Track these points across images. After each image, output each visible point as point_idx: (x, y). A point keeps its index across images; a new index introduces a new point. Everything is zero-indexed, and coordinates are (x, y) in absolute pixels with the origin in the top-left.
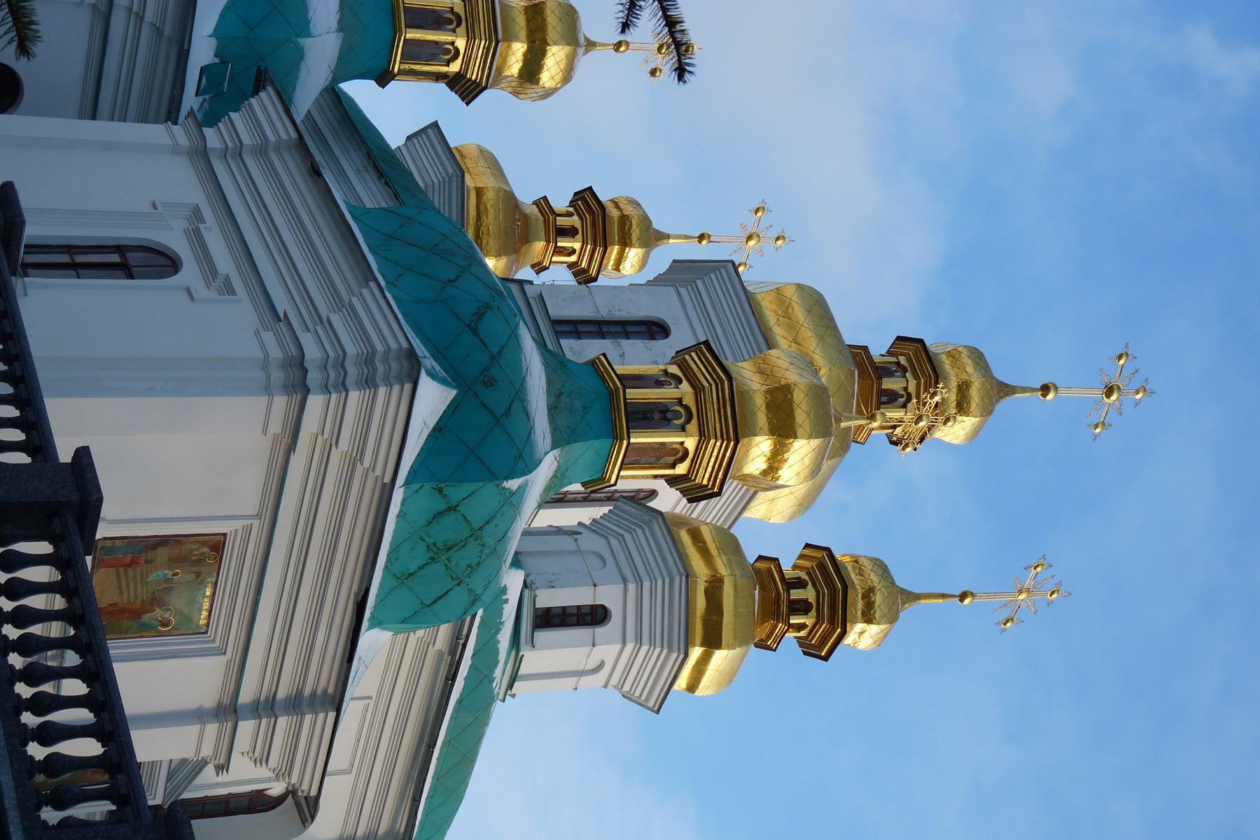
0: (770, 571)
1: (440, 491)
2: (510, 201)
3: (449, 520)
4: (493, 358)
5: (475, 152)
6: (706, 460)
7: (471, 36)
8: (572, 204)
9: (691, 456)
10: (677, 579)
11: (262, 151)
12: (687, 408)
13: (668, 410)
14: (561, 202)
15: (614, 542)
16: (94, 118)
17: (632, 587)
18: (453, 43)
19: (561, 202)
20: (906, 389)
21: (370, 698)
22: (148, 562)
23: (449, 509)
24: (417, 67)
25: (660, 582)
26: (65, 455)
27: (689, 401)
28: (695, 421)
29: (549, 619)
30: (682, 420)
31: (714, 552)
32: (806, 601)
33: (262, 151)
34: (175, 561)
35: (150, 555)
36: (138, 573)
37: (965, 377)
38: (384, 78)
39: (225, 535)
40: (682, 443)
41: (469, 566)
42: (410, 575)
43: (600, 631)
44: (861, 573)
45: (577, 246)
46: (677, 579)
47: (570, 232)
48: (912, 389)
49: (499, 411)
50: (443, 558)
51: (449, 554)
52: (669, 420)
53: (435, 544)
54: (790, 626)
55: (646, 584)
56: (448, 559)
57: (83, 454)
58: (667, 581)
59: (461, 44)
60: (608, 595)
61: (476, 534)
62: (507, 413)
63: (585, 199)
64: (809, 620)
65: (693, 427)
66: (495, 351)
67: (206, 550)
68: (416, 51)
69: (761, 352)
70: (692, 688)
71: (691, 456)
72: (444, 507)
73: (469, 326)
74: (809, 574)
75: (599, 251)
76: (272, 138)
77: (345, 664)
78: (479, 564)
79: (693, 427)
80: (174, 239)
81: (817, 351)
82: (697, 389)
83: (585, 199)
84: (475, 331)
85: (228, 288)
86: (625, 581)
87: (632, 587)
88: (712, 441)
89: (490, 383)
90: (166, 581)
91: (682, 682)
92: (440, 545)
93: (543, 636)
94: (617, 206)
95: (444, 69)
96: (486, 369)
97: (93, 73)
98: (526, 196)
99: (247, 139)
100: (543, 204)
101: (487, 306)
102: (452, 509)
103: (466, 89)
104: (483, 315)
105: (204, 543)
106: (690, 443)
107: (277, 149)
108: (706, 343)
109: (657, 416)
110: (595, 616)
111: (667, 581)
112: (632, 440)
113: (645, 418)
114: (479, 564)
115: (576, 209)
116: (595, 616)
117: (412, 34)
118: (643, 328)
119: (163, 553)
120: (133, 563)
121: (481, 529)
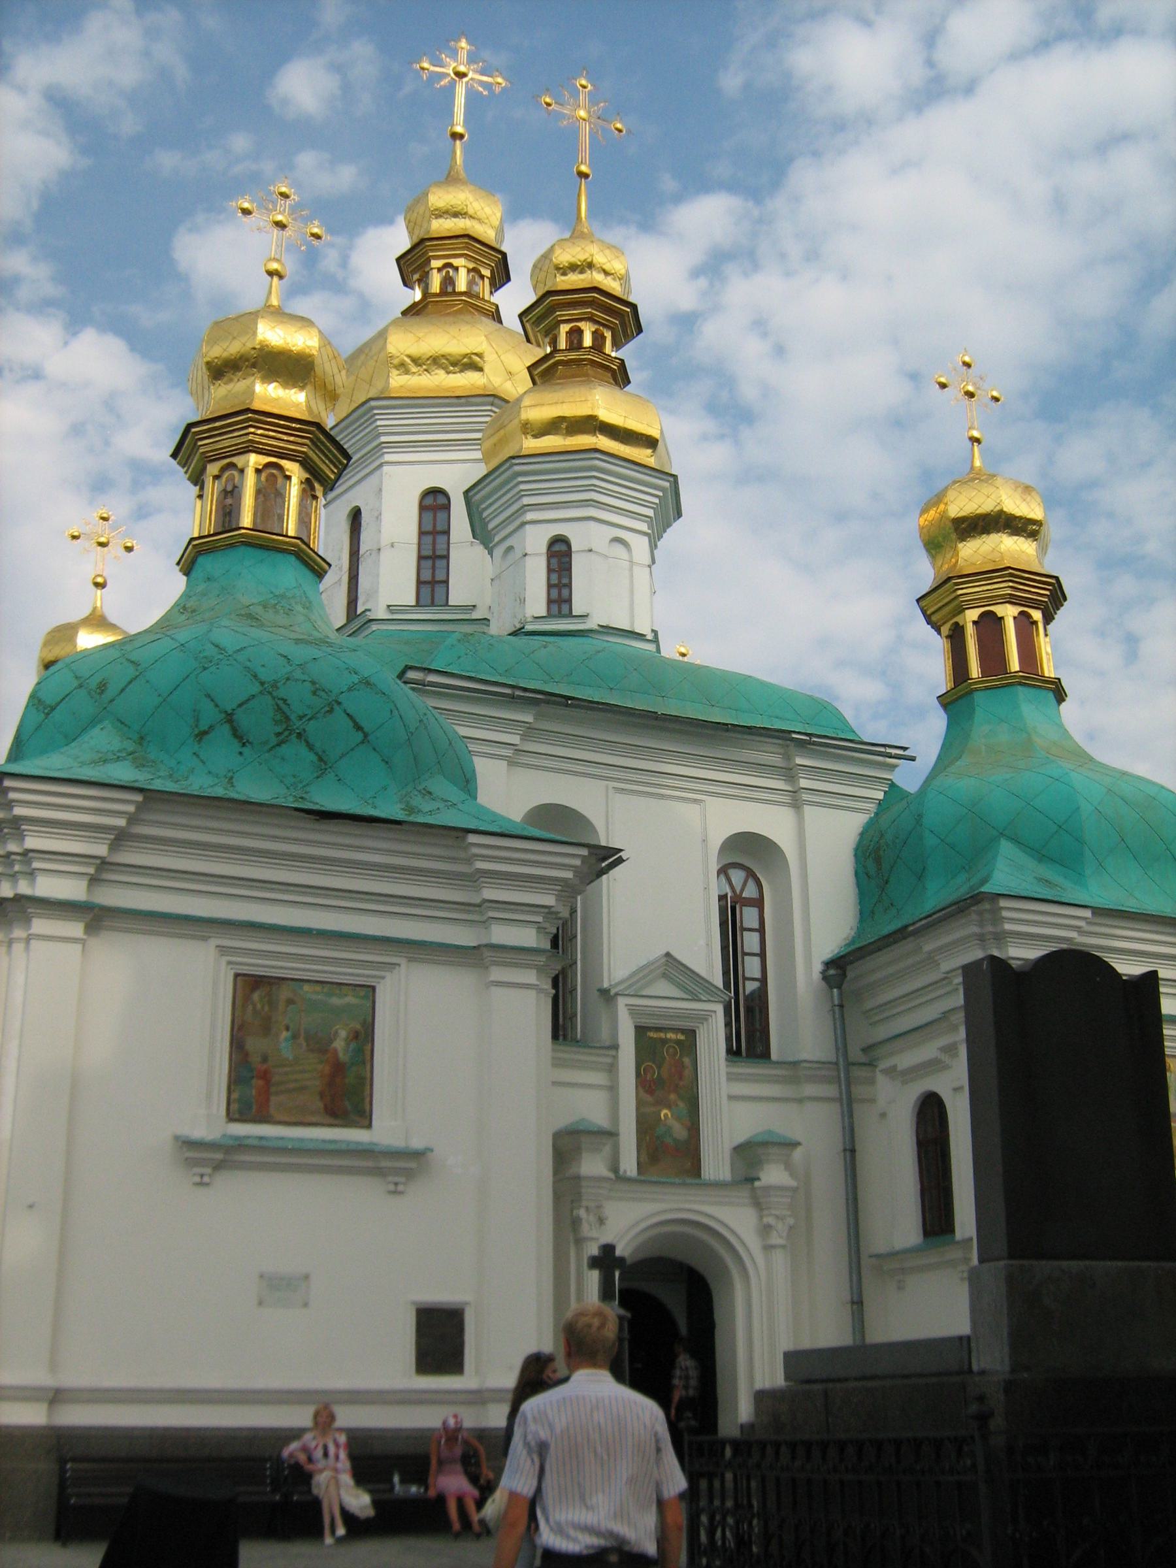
3: (244, 720)
10: (517, 468)
20: (439, 270)
21: (607, 787)
22: (265, 1059)
25: (522, 487)
28: (234, 460)
29: (560, 594)
30: (235, 473)
32: (570, 333)
34: (267, 1028)
35: (255, 1059)
41: (314, 693)
42: (321, 759)
49: (131, 672)
50: (298, 723)
51: (293, 717)
52: (235, 487)
53: (278, 734)
55: (526, 501)
56: (301, 718)
58: (520, 479)
60: (536, 540)
61: (269, 688)
62: (136, 664)
64: (588, 330)
65: (239, 461)
66: (76, 683)
67: (256, 996)
72: (227, 727)
73: (48, 714)
76: (569, 875)
77: (404, 827)
78: (313, 683)
79: (239, 461)
84: (53, 709)
86: (523, 524)
87: (530, 516)
89: (102, 687)
90: (295, 1037)
91: (641, 454)
92: (279, 729)
102: (229, 718)
104: (40, 701)
105: (247, 999)
109: (229, 501)
110: (560, 554)
111: (520, 479)
112: (291, 533)
113: (230, 513)
114: (313, 683)
116: (560, 554)
119: (255, 1044)
120: (265, 1076)
121: (262, 684)
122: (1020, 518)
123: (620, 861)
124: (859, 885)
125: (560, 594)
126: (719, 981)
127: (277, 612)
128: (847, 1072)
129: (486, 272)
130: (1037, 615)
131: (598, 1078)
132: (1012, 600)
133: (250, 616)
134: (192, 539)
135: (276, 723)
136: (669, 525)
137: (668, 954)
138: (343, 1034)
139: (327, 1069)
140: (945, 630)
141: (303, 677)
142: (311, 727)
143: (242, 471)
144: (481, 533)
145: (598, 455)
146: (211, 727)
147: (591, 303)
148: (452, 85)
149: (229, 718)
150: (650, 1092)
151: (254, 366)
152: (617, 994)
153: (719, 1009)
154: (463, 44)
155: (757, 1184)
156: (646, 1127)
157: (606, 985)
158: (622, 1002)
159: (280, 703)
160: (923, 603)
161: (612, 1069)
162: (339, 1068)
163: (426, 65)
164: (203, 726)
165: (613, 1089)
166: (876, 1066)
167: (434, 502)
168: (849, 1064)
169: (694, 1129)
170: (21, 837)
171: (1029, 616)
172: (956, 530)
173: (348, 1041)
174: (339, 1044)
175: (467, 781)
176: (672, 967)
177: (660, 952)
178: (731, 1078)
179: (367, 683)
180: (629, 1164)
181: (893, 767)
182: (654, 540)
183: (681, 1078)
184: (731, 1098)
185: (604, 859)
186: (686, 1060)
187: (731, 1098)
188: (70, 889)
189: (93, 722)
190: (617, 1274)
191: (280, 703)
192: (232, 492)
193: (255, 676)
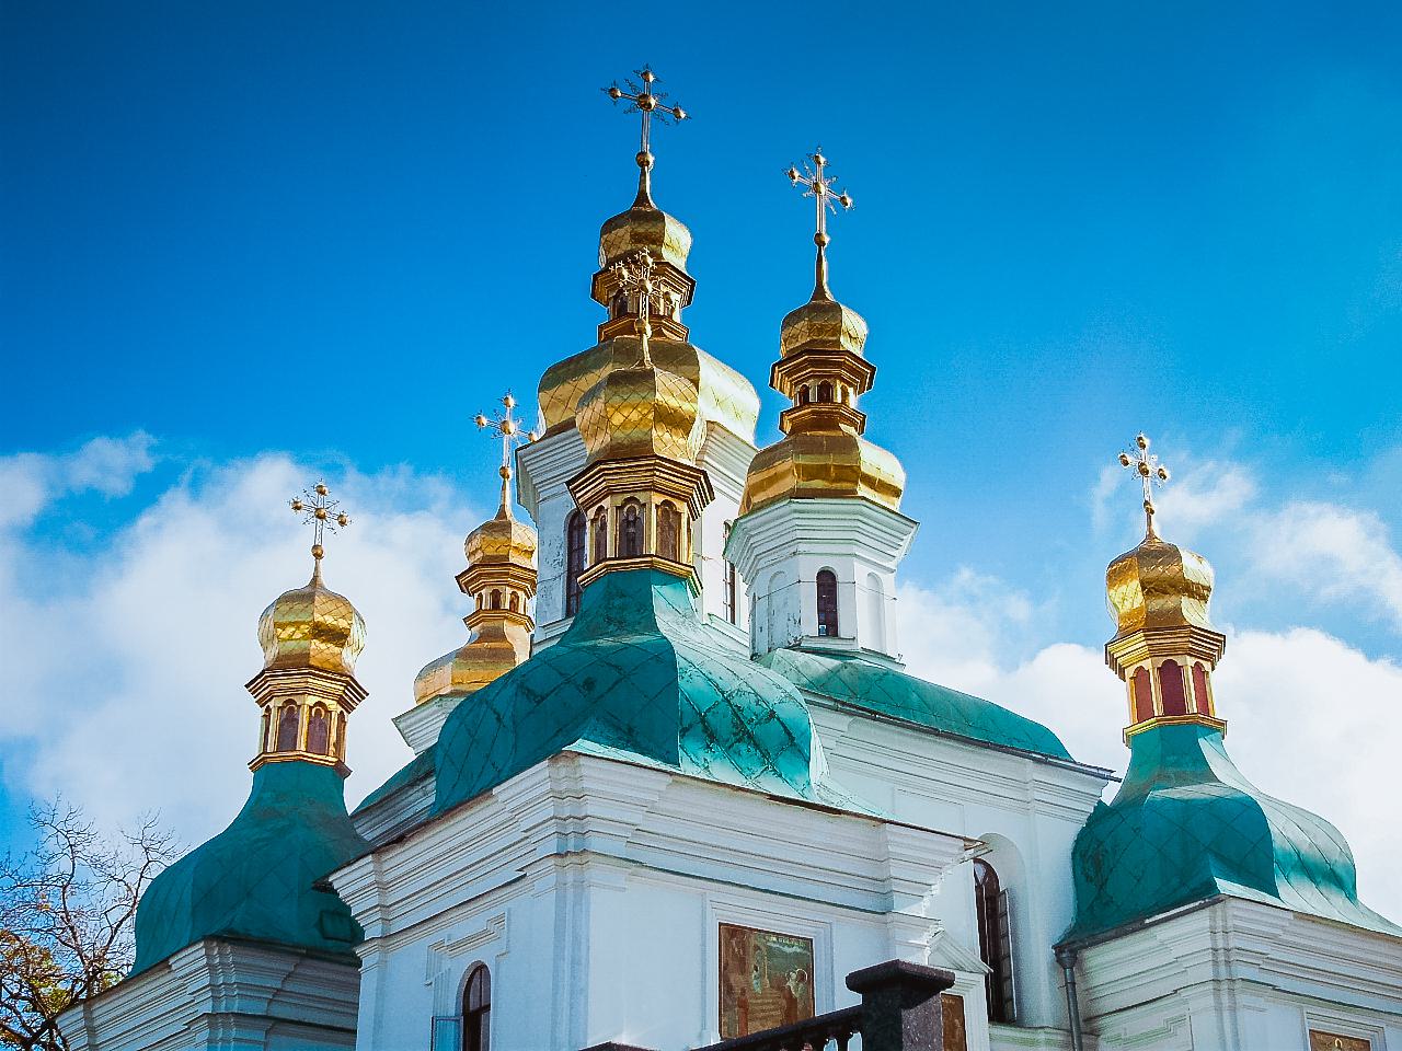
0: (791, 420)
2: (464, 655)
4: (568, 681)
5: (421, 684)
6: (669, 484)
7: (306, 692)
8: (471, 594)
9: (669, 498)
11: (383, 887)
12: (628, 501)
13: (627, 519)
14: (469, 604)
15: (762, 564)
16: (354, 1032)
18: (311, 708)
19: (469, 604)
21: (893, 789)
22: (743, 991)
24: (333, 738)
26: (855, 999)
27: (619, 500)
31: (772, 472)
33: (383, 887)
34: (743, 970)
37: (628, 237)
38: (341, 771)
39: (720, 924)
40: (657, 506)
43: (840, 578)
44: (795, 337)
45: (509, 590)
46: (794, 506)
47: (496, 596)
49: (615, 675)
52: (636, 518)
53: (735, 734)
54: (843, 402)
57: (854, 982)
59: (311, 700)
60: (808, 571)
63: (466, 582)
65: (642, 497)
68: (318, 741)
69: (789, 374)
71: (669, 498)
72: (700, 725)
73: (539, 702)
74: (796, 384)
75: (514, 571)
78: (756, 694)
80: (457, 969)
81: (597, 372)
82: (610, 492)
83: (466, 582)
84: (543, 699)
85: (499, 920)
87: (802, 547)
88: (655, 478)
89: (589, 684)
94: (473, 553)
95: (335, 716)
96: (577, 687)
97: (326, 1034)
98: (462, 637)
99: (375, 901)
100: (470, 621)
101: (521, 686)
103: (352, 694)
104: (529, 690)
105: (728, 944)
106: (658, 499)
107: (382, 873)
108: (568, 483)
109: (632, 530)
110: (827, 583)
112: (653, 552)
113: (633, 540)
115: (475, 592)
116: (827, 583)
117: (302, 746)
118: (575, 533)
119: (736, 979)
120: (743, 1005)
124: (1076, 884)
128: (1080, 1039)
135: (735, 725)
138: (794, 976)
140: (1130, 672)
145: (864, 502)
146: (691, 726)
162: (792, 1001)
164: (686, 724)
166: (1099, 1036)
172: (1143, 588)
174: (791, 984)
183: (953, 1037)
192: (634, 522)
193: (717, 686)
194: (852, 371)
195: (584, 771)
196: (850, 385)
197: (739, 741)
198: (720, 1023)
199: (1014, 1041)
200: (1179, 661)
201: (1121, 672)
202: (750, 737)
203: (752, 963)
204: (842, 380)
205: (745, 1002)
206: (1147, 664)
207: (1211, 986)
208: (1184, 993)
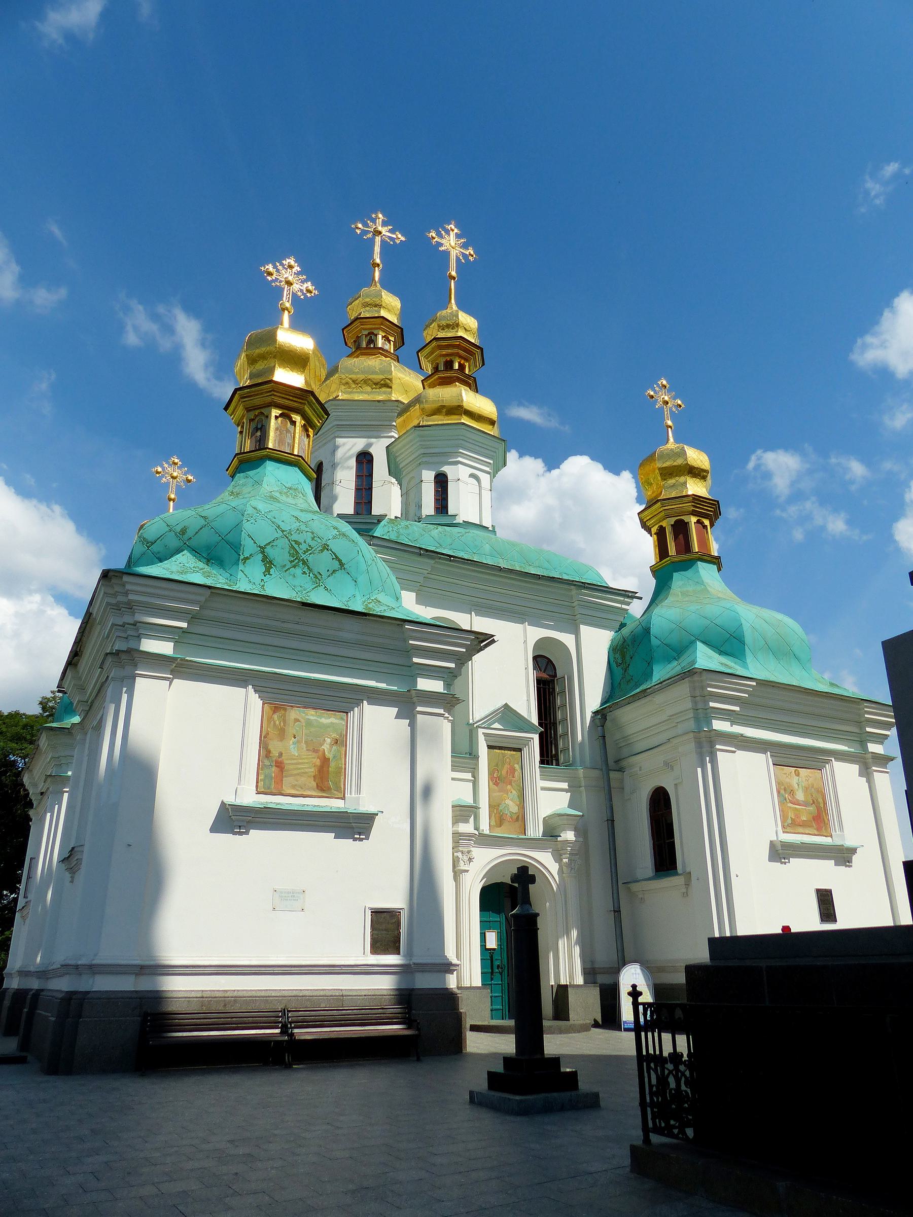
1: (246, 559)
17: (460, 459)
20: (366, 336)
22: (281, 754)
23: (263, 552)
28: (263, 410)
29: (442, 504)
34: (282, 734)
35: (275, 753)
36: (290, 762)
40: (276, 417)
42: (316, 577)
48: (366, 332)
49: (203, 522)
51: (300, 552)
53: (291, 562)
61: (286, 534)
62: (205, 518)
66: (167, 529)
67: (275, 716)
70: (492, 423)
78: (313, 533)
84: (152, 543)
89: (183, 531)
93: (451, 511)
105: (270, 719)
110: (441, 482)
112: (296, 453)
114: (313, 533)
119: (275, 747)
120: (280, 765)
121: (283, 531)
122: (697, 468)
123: (493, 641)
125: (442, 504)
126: (535, 720)
127: (288, 496)
129: (392, 339)
130: (707, 522)
131: (469, 776)
132: (694, 513)
133: (272, 497)
134: (237, 454)
135: (291, 555)
136: (499, 470)
137: (506, 706)
138: (328, 740)
139: (318, 762)
140: (654, 530)
141: (307, 529)
142: (310, 559)
143: (267, 417)
144: (394, 470)
147: (458, 347)
148: (372, 241)
149: (262, 549)
150: (496, 784)
151: (275, 357)
152: (478, 727)
153: (536, 738)
154: (380, 216)
155: (559, 839)
156: (493, 807)
157: (471, 721)
158: (481, 731)
159: (293, 543)
160: (642, 515)
161: (474, 771)
162: (325, 761)
163: (360, 226)
165: (475, 783)
167: (365, 459)
168: (609, 770)
169: (522, 807)
170: (133, 614)
171: (702, 523)
173: (331, 745)
174: (326, 747)
175: (397, 599)
176: (507, 715)
177: (500, 704)
178: (544, 777)
179: (344, 535)
180: (485, 827)
181: (628, 604)
182: (493, 474)
184: (543, 789)
185: (483, 641)
186: (517, 767)
187: (543, 789)
188: (165, 648)
189: (178, 551)
190: (39, 959)
191: (293, 543)
192: (261, 429)
194: (466, 350)
195: (128, 587)
196: (466, 360)
197: (294, 567)
198: (257, 779)
199: (282, 805)
200: (685, 518)
201: (649, 532)
202: (305, 563)
203: (291, 731)
204: (460, 357)
205: (282, 763)
206: (664, 524)
207: (692, 735)
208: (675, 741)
